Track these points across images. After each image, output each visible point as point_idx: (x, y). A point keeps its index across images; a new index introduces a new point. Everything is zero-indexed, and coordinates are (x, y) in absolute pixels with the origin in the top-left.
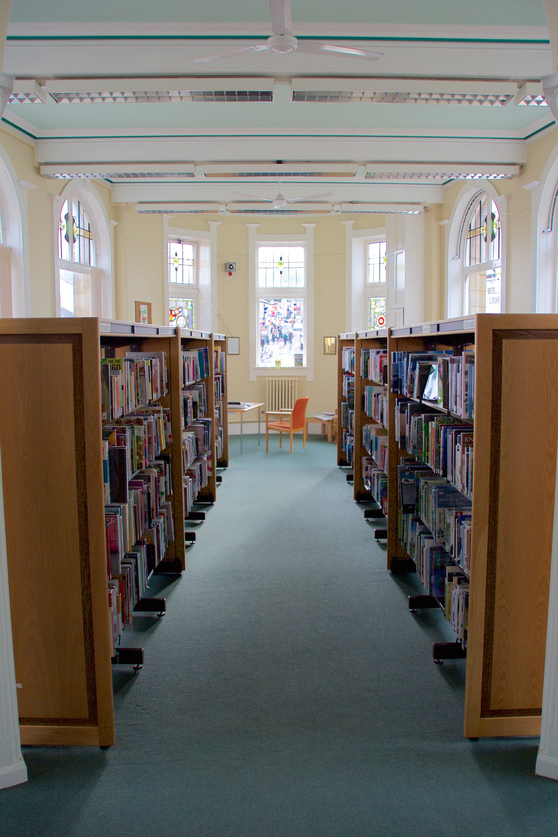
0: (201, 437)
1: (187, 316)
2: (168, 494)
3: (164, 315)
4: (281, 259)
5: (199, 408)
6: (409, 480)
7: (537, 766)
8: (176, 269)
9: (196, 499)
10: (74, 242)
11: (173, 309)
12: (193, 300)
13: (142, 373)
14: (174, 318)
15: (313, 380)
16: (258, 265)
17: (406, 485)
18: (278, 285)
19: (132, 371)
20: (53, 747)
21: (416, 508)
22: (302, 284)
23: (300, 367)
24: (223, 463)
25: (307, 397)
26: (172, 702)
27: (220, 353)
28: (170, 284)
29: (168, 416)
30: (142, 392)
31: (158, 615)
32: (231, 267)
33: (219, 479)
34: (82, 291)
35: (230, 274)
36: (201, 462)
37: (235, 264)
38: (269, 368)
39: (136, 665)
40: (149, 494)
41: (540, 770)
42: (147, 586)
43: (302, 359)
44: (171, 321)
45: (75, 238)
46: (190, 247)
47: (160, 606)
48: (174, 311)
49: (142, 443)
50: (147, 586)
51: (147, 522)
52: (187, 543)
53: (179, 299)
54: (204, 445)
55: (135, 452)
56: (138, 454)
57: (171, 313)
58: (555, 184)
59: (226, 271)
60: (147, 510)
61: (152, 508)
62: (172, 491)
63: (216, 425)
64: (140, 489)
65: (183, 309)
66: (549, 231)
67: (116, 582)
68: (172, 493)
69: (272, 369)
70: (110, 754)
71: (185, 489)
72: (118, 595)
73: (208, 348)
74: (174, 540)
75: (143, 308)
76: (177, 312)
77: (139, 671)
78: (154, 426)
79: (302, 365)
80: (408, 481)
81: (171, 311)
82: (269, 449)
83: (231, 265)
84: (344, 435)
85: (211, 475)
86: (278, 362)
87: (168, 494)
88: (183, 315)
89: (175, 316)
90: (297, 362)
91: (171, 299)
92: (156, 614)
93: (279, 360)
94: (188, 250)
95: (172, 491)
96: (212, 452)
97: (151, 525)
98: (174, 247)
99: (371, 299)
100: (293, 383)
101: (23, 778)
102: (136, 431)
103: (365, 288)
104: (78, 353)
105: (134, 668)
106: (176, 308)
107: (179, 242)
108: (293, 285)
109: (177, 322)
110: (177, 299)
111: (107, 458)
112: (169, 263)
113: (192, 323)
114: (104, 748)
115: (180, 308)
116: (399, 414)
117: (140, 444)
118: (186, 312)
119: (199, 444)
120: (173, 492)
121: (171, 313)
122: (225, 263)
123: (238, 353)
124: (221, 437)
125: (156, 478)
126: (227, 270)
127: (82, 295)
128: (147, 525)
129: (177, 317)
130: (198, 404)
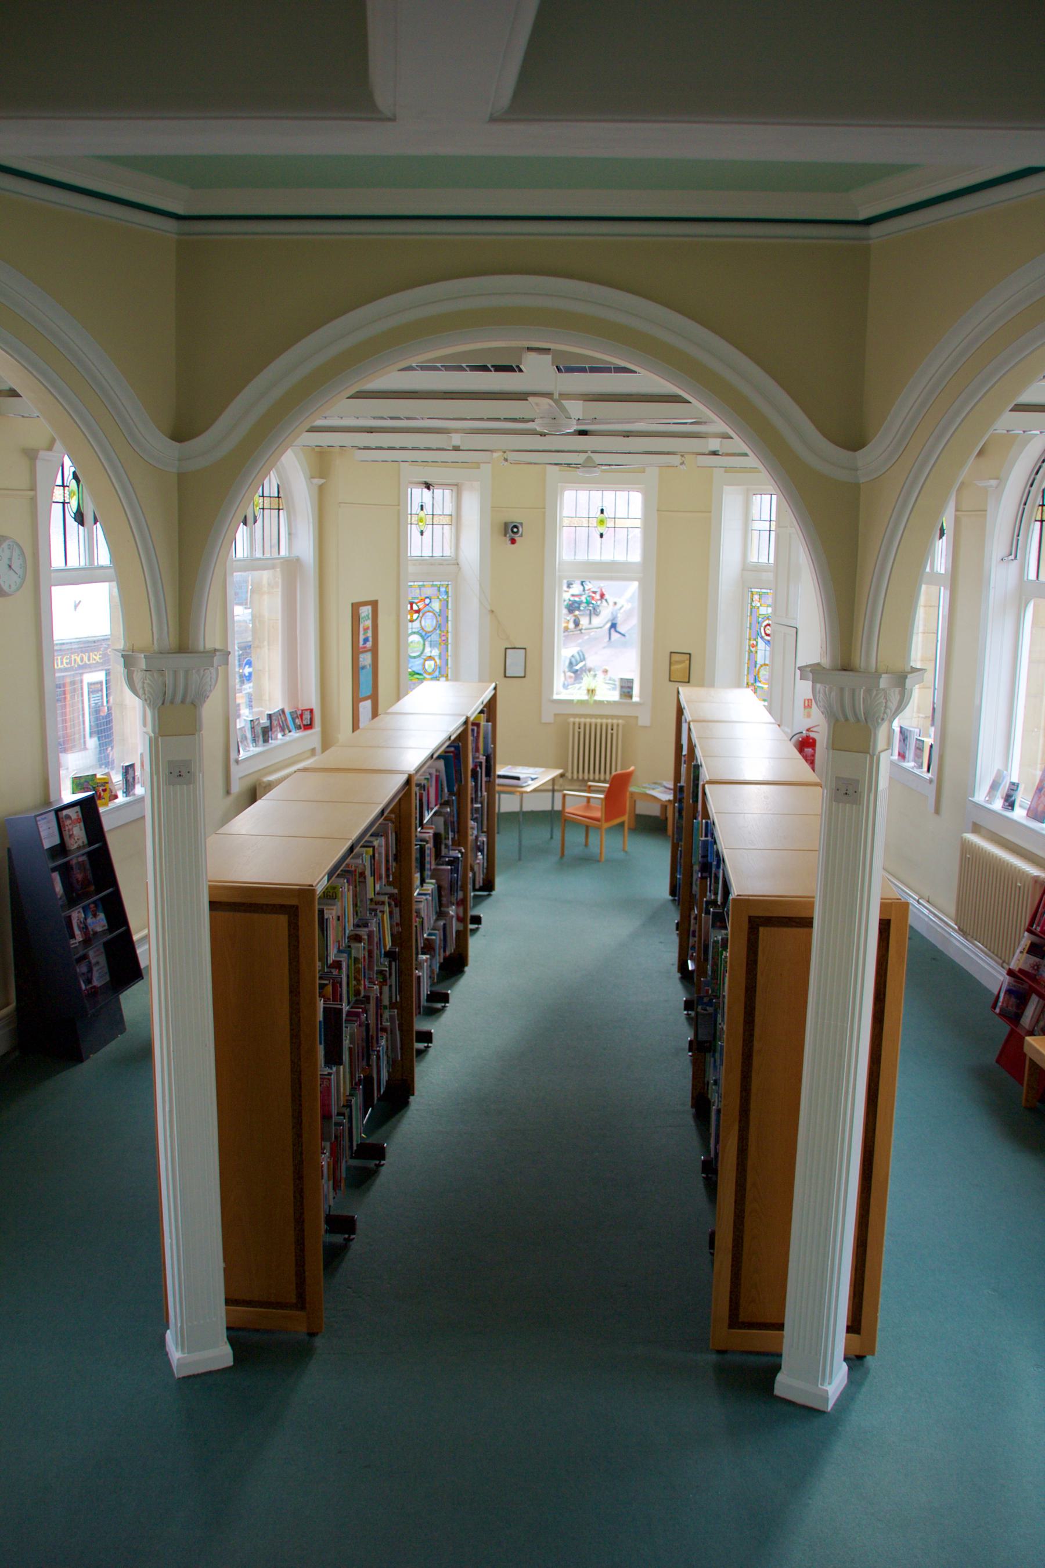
0: (446, 884)
1: (438, 611)
2: (394, 1001)
3: (398, 616)
4: (602, 511)
5: (444, 842)
6: (708, 1008)
7: (776, 1386)
8: (422, 533)
9: (435, 980)
10: (255, 521)
11: (416, 601)
12: (450, 583)
13: (362, 879)
14: (415, 616)
15: (648, 724)
16: (561, 521)
17: (703, 1015)
18: (595, 557)
19: (349, 885)
20: (257, 1330)
21: (713, 1047)
22: (635, 556)
23: (628, 701)
24: (488, 886)
25: (632, 768)
26: (389, 1286)
27: (484, 725)
28: (409, 558)
29: (395, 900)
30: (361, 901)
31: (376, 1165)
32: (515, 530)
33: (477, 920)
34: (265, 589)
35: (513, 541)
36: (446, 920)
37: (521, 524)
38: (575, 701)
39: (347, 1236)
40: (368, 1025)
41: (779, 1391)
42: (363, 1135)
43: (631, 688)
44: (412, 621)
45: (256, 514)
46: (447, 492)
47: (378, 1152)
48: (416, 603)
49: (360, 966)
50: (363, 1135)
51: (365, 1059)
52: (421, 1046)
53: (425, 583)
54: (451, 894)
55: (352, 975)
56: (356, 978)
57: (412, 608)
58: (1040, 454)
59: (505, 536)
60: (364, 1044)
61: (372, 1036)
62: (398, 996)
63: (471, 850)
64: (356, 1021)
65: (433, 600)
66: (1012, 560)
67: (328, 1145)
68: (398, 999)
69: (581, 703)
70: (319, 1342)
71: (419, 977)
72: (328, 1160)
73: (460, 744)
74: (399, 1058)
75: (366, 611)
76: (421, 605)
77: (351, 1243)
78: (376, 934)
79: (631, 697)
80: (706, 1010)
81: (411, 604)
82: (566, 852)
83: (515, 527)
84: (679, 852)
85: (461, 928)
86: (591, 692)
87: (394, 1001)
88: (431, 610)
89: (418, 612)
90: (624, 692)
91: (412, 584)
92: (372, 1164)
93: (593, 688)
94: (441, 499)
95: (398, 996)
96: (464, 894)
97: (373, 642)
98: (419, 495)
99: (753, 590)
100: (615, 728)
101: (229, 1361)
102: (353, 952)
103: (743, 570)
104: (294, 927)
105: (345, 1239)
106: (420, 598)
107: (428, 486)
108: (620, 557)
109: (421, 623)
110: (421, 583)
111: (321, 1019)
112: (409, 512)
113: (447, 621)
114: (312, 1335)
115: (428, 598)
116: (703, 915)
117: (359, 967)
118: (436, 606)
119: (443, 893)
120: (401, 998)
121: (412, 608)
122: (504, 521)
123: (523, 675)
124: (483, 854)
125: (377, 997)
126: (508, 536)
127: (266, 597)
128: (365, 1063)
129: (421, 614)
130: (443, 836)
